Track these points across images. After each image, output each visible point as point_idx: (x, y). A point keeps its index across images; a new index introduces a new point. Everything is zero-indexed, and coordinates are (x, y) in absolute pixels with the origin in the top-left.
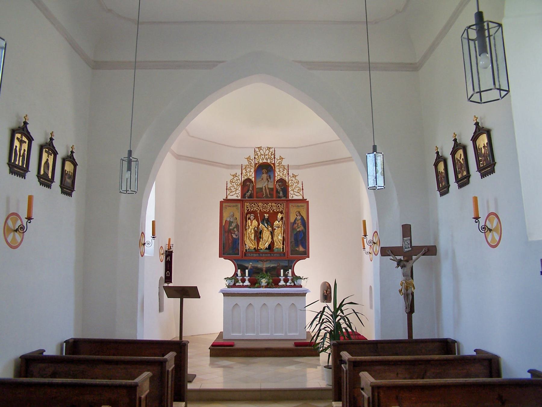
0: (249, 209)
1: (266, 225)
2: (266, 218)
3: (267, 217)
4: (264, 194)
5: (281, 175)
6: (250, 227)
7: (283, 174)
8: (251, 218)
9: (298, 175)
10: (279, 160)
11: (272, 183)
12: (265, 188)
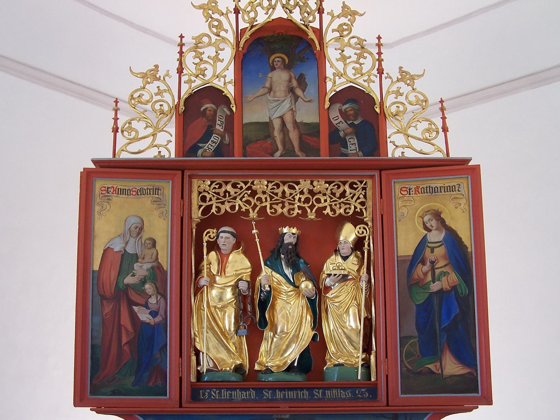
0: (210, 207)
1: (288, 272)
2: (290, 244)
3: (293, 240)
4: (280, 146)
5: (350, 72)
6: (217, 278)
7: (359, 71)
8: (221, 242)
9: (422, 75)
10: (338, 16)
11: (315, 105)
12: (283, 124)
